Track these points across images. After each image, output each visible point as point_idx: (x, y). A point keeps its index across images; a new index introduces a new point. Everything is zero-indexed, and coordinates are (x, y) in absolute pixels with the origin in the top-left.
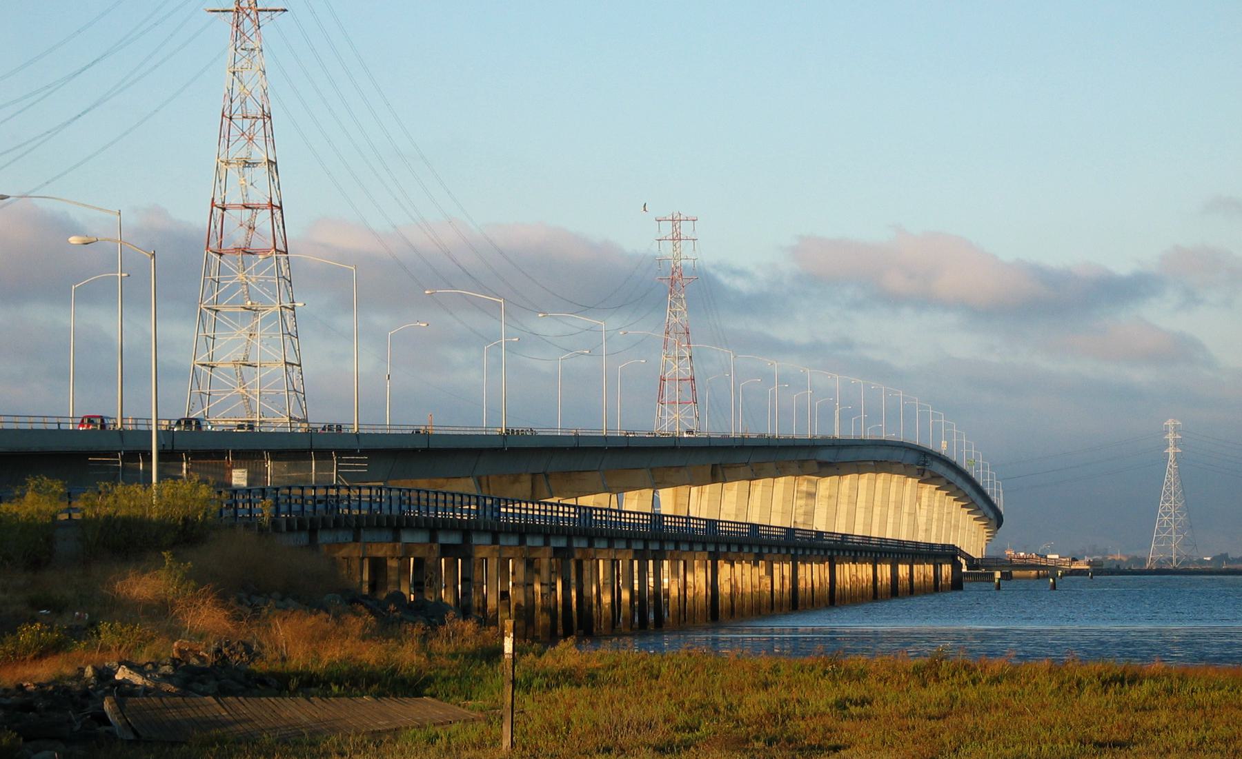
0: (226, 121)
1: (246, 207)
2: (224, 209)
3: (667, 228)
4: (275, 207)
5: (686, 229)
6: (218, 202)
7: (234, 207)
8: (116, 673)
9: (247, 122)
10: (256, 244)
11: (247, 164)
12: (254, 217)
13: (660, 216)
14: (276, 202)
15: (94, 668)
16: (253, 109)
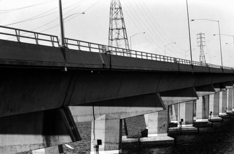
0: (111, 10)
1: (117, 29)
2: (112, 40)
3: (199, 36)
4: (124, 29)
5: (203, 36)
6: (111, 28)
7: (114, 29)
8: (122, 151)
9: (116, 10)
10: (120, 37)
11: (116, 19)
12: (119, 31)
13: (198, 34)
14: (124, 27)
15: (67, 68)
16: (117, 7)
